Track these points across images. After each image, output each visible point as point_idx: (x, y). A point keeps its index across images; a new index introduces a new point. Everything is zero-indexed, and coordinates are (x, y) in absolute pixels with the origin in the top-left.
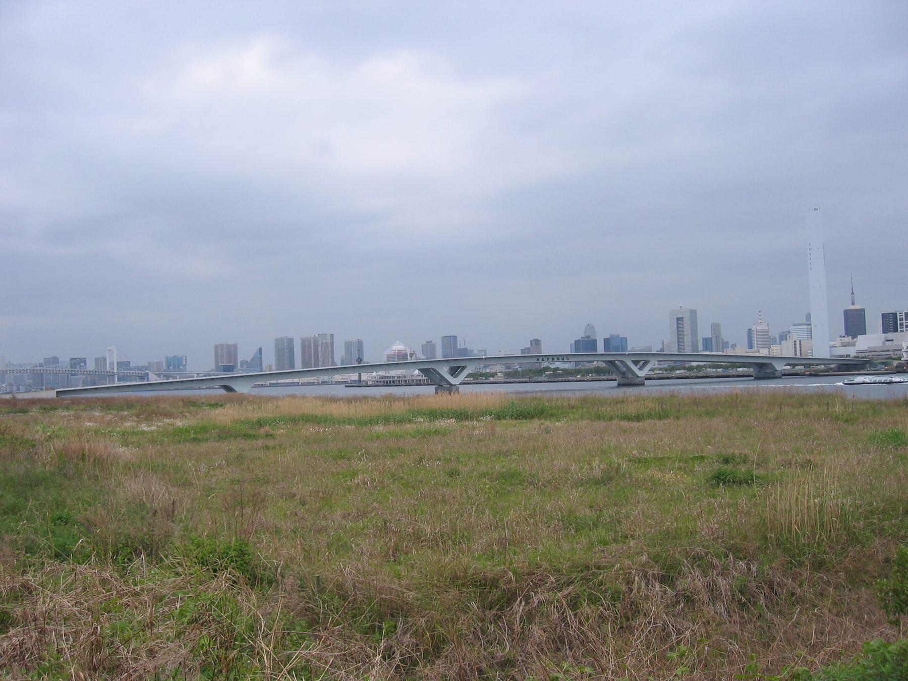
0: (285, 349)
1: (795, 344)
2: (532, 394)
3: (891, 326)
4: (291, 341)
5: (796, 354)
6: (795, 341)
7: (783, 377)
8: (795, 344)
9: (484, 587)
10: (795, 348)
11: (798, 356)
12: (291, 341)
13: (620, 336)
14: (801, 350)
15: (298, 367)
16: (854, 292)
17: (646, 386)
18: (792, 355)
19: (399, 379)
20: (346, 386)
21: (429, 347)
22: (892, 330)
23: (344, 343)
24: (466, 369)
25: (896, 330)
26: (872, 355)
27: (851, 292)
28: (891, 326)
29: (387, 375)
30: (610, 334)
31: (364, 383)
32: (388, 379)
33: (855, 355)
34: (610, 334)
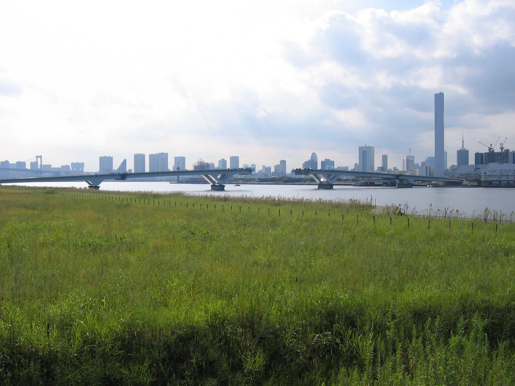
0: (139, 159)
1: (427, 169)
2: (92, 194)
3: (480, 161)
4: (143, 156)
5: (427, 174)
6: (427, 167)
7: (413, 187)
8: (427, 169)
9: (212, 302)
10: (427, 171)
11: (428, 175)
12: (143, 156)
13: (330, 160)
14: (430, 171)
15: (147, 170)
16: (464, 141)
17: (226, 191)
18: (424, 175)
19: (200, 180)
20: (170, 183)
21: (223, 162)
22: (480, 163)
23: (434, 95)
24: (429, 156)
25: (482, 163)
26: (468, 177)
27: (462, 140)
28: (480, 161)
29: (194, 177)
30: (264, 166)
31: (219, 177)
32: (194, 180)
33: (458, 176)
34: (264, 166)
